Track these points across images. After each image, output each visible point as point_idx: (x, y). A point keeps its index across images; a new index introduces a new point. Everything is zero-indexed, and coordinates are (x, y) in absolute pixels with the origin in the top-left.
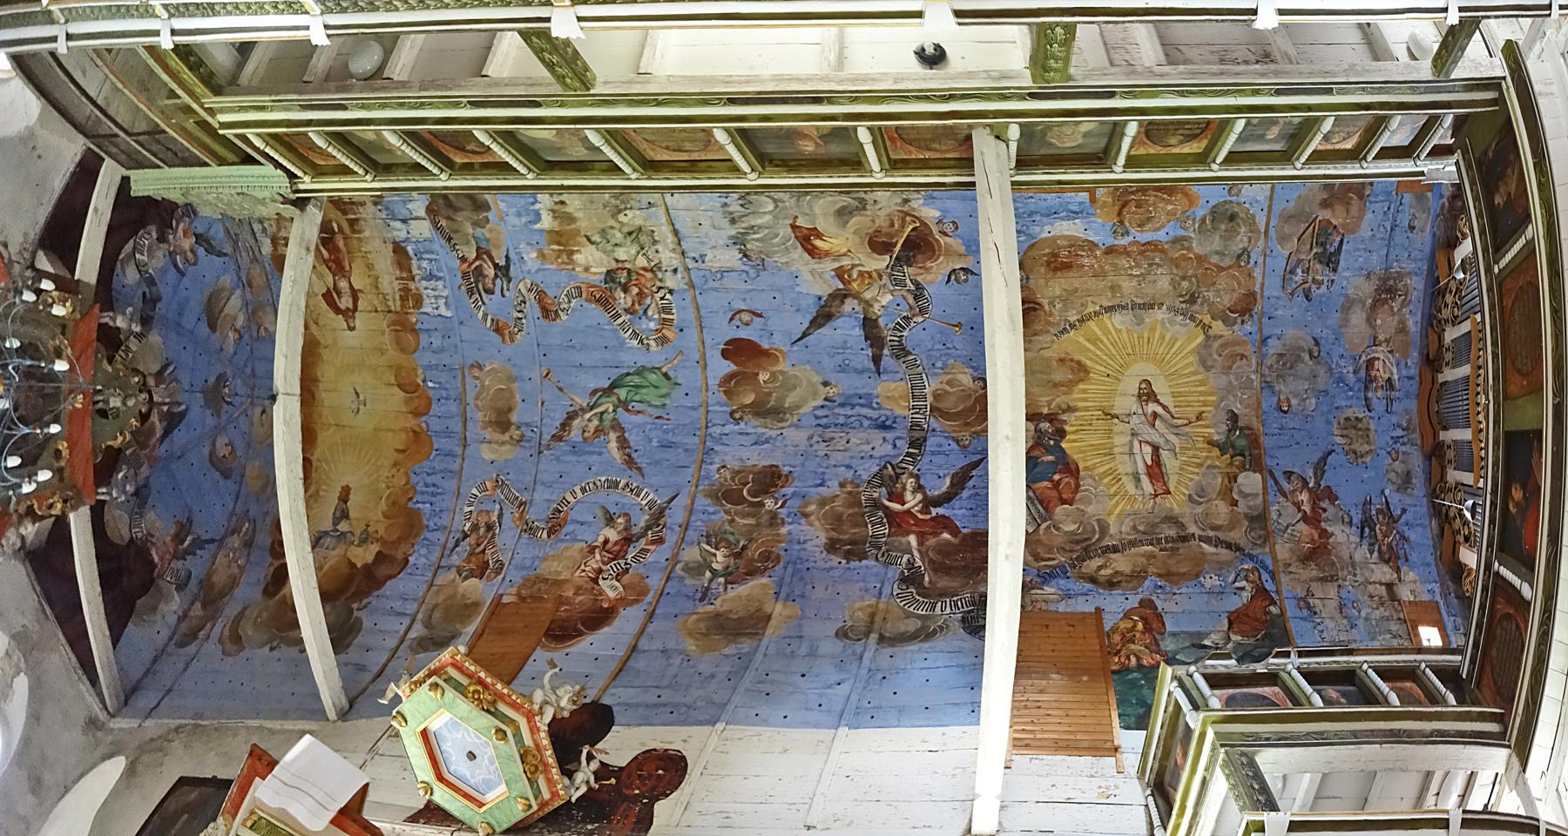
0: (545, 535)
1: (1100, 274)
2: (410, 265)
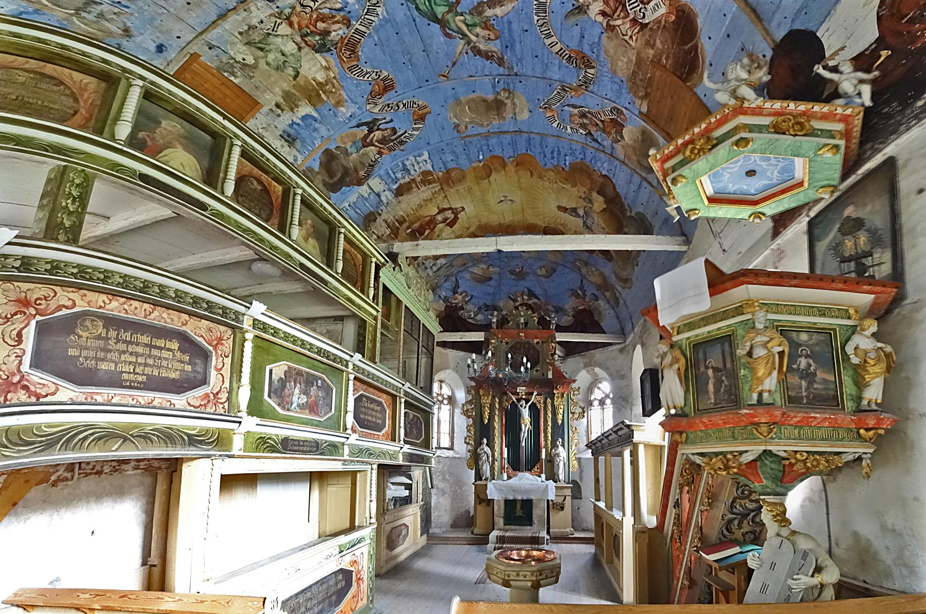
0: (592, 71)
2: (406, 184)
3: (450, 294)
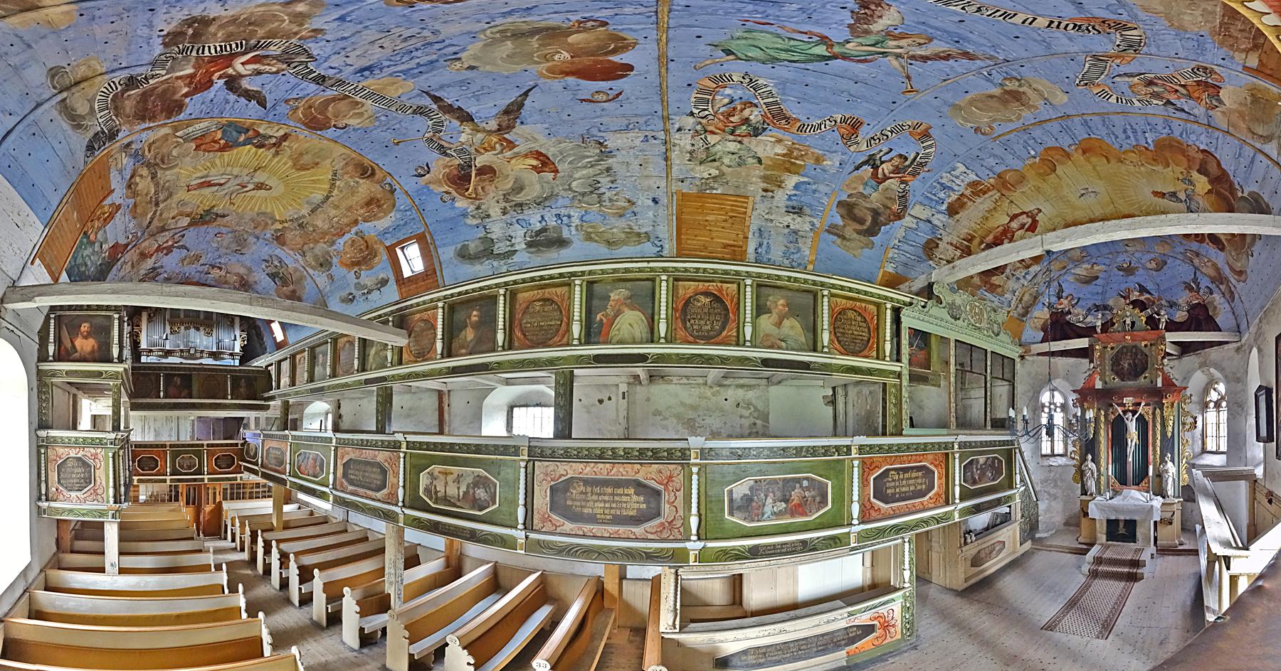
1: (350, 209)
3: (1054, 299)
